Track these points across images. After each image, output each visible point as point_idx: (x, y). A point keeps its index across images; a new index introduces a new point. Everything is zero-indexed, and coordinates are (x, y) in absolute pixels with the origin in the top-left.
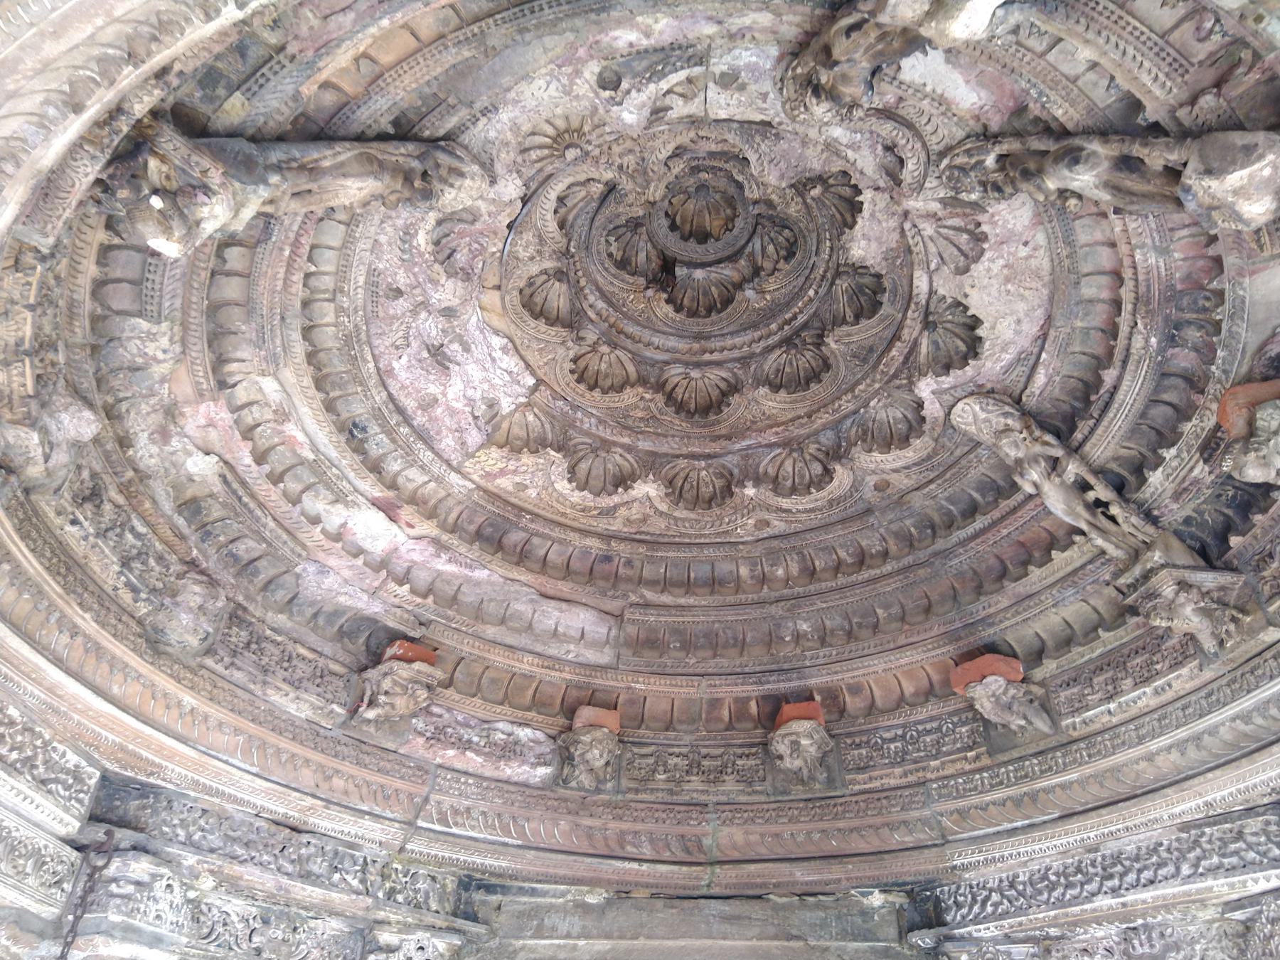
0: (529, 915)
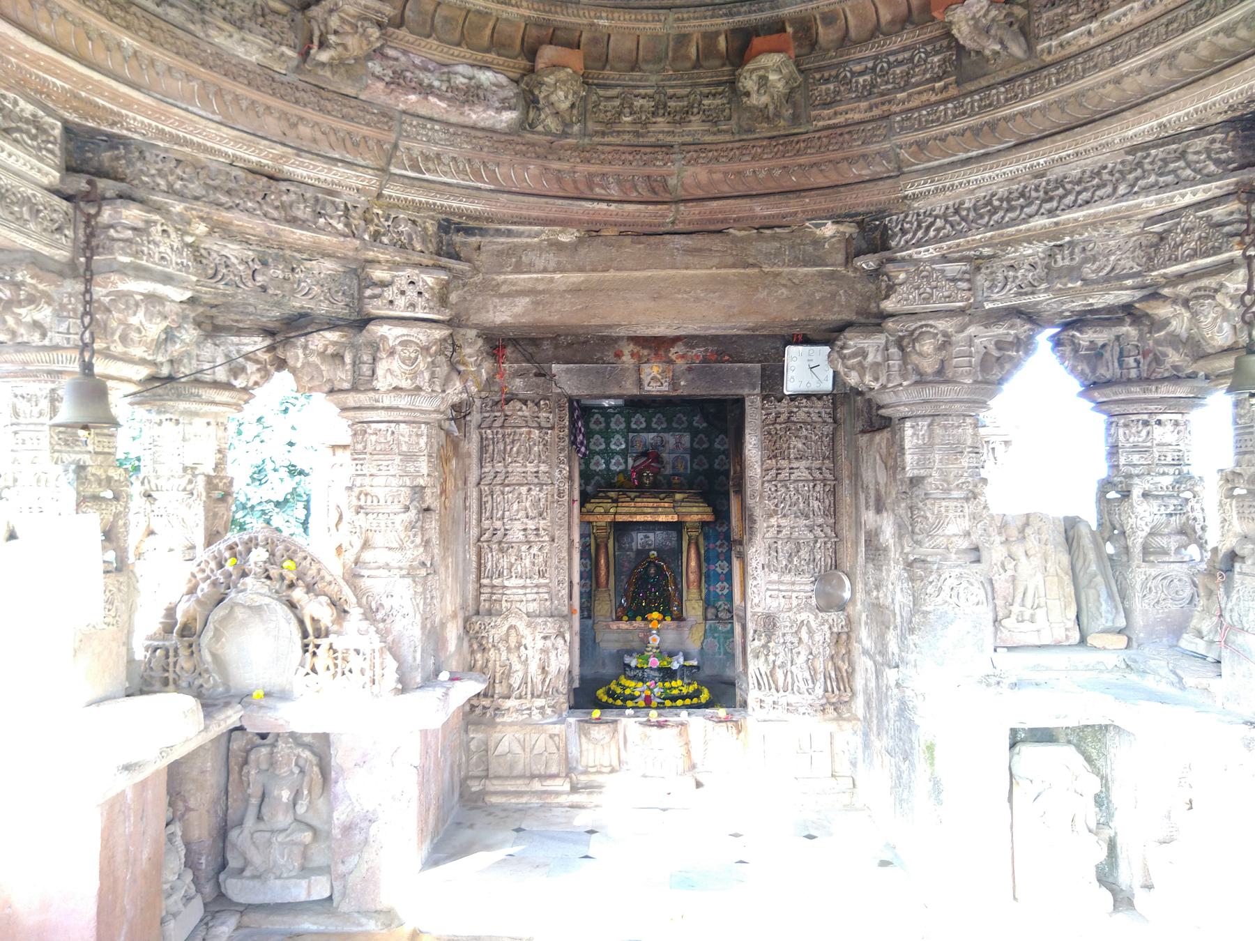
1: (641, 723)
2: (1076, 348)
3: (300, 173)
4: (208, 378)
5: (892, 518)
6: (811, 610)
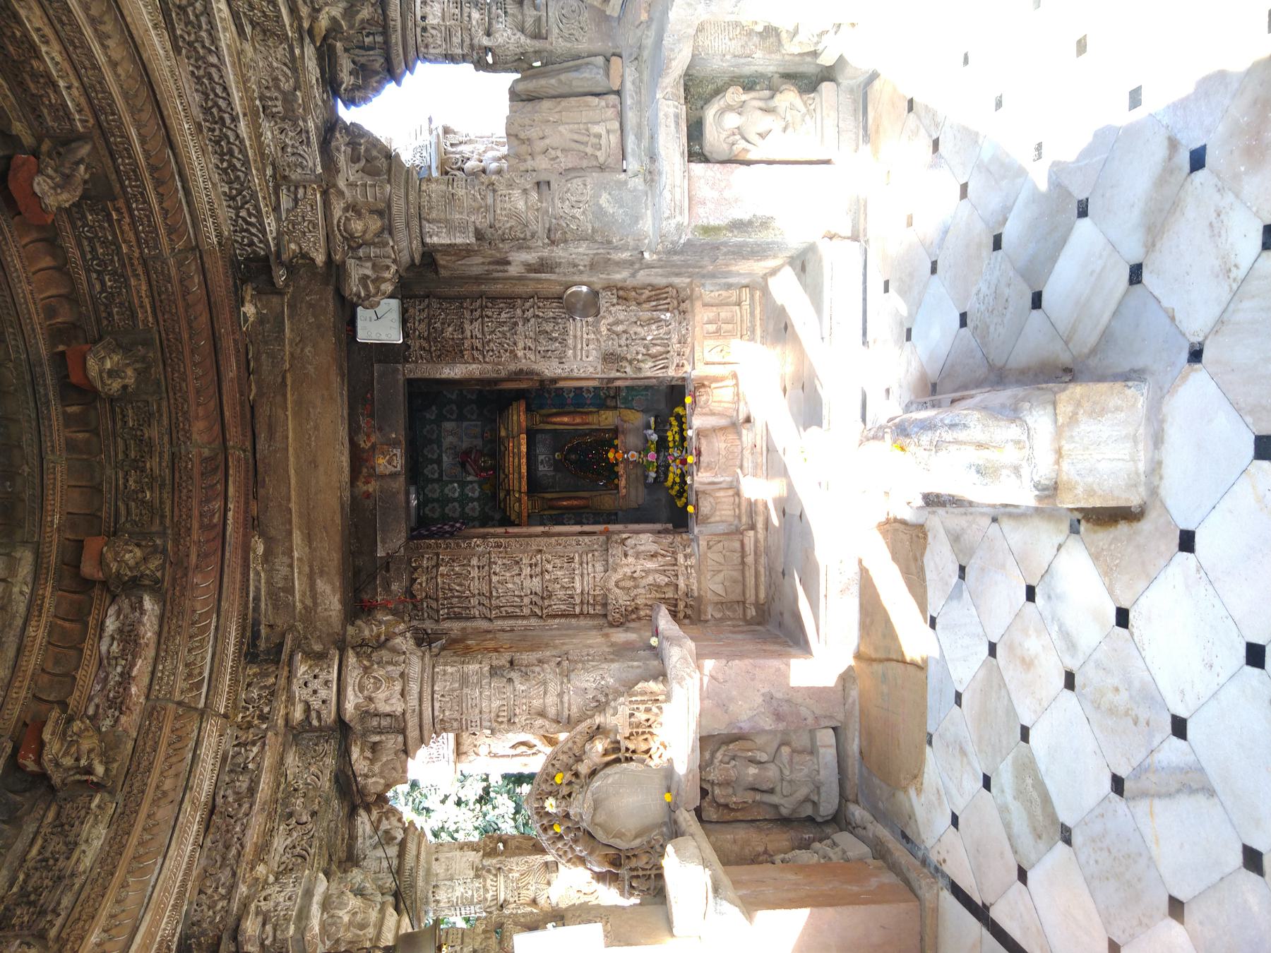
0: (276, 600)
1: (698, 471)
2: (357, 88)
3: (207, 787)
4: (395, 862)
5: (513, 254)
6: (598, 322)
